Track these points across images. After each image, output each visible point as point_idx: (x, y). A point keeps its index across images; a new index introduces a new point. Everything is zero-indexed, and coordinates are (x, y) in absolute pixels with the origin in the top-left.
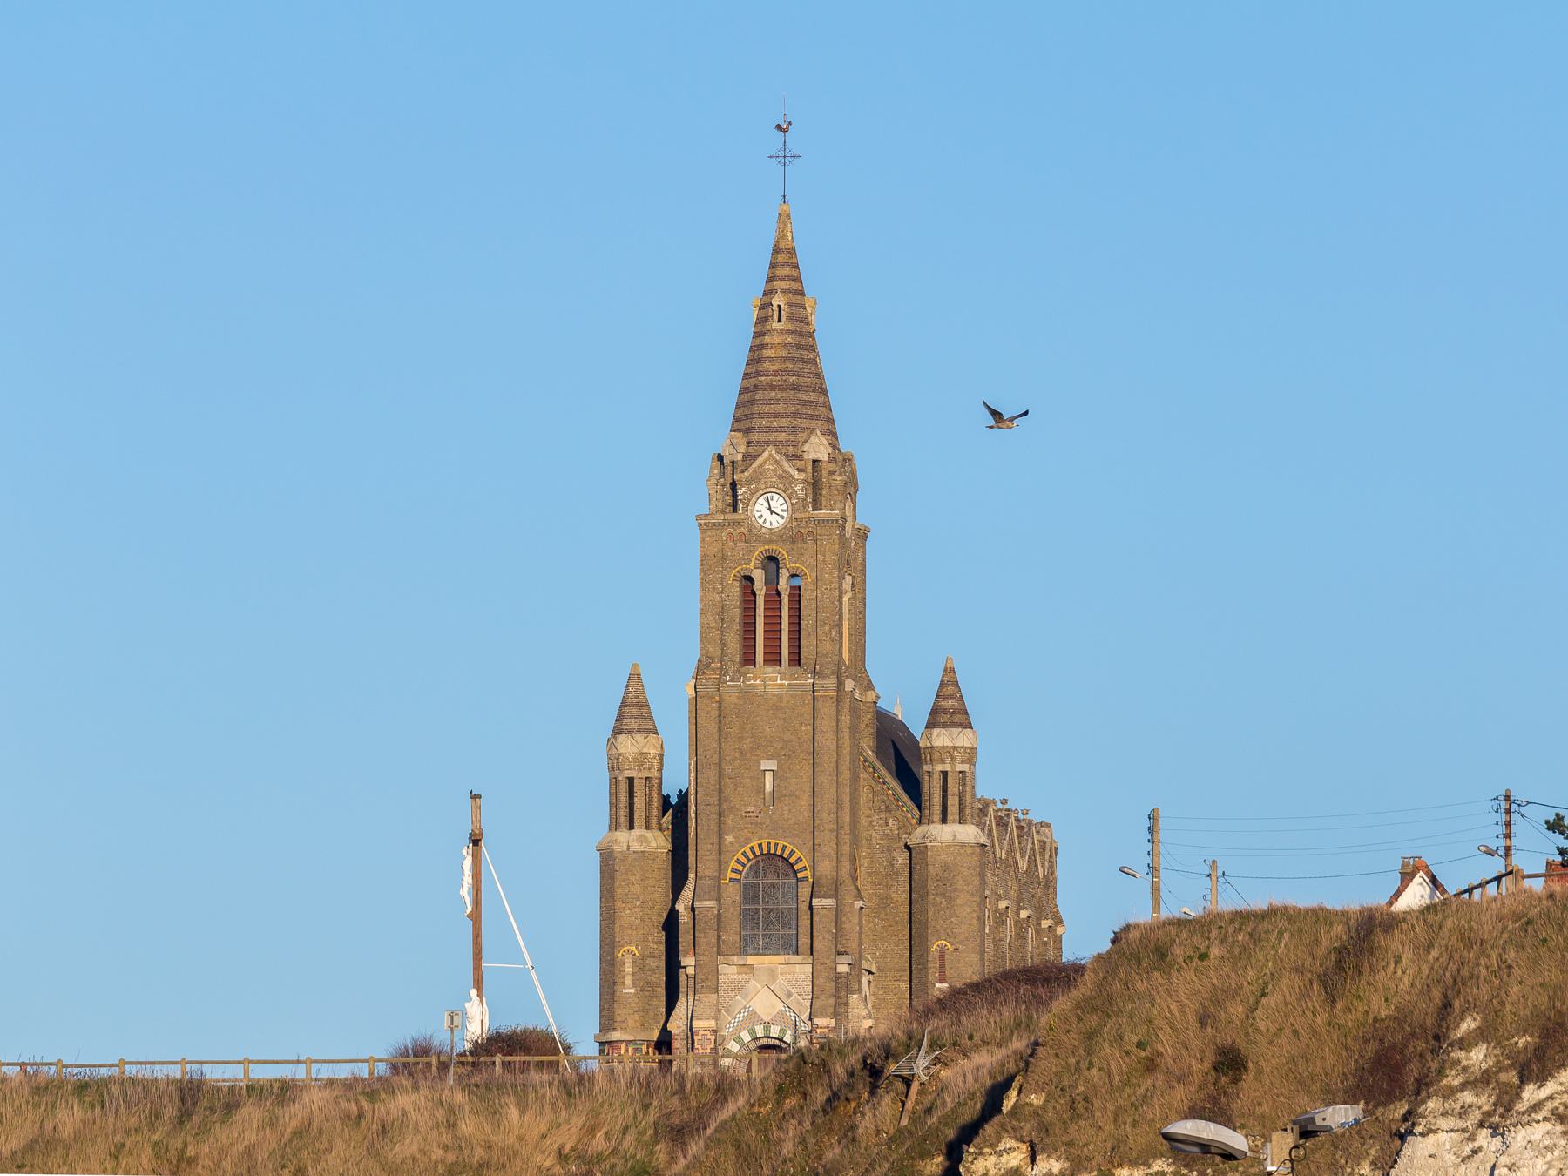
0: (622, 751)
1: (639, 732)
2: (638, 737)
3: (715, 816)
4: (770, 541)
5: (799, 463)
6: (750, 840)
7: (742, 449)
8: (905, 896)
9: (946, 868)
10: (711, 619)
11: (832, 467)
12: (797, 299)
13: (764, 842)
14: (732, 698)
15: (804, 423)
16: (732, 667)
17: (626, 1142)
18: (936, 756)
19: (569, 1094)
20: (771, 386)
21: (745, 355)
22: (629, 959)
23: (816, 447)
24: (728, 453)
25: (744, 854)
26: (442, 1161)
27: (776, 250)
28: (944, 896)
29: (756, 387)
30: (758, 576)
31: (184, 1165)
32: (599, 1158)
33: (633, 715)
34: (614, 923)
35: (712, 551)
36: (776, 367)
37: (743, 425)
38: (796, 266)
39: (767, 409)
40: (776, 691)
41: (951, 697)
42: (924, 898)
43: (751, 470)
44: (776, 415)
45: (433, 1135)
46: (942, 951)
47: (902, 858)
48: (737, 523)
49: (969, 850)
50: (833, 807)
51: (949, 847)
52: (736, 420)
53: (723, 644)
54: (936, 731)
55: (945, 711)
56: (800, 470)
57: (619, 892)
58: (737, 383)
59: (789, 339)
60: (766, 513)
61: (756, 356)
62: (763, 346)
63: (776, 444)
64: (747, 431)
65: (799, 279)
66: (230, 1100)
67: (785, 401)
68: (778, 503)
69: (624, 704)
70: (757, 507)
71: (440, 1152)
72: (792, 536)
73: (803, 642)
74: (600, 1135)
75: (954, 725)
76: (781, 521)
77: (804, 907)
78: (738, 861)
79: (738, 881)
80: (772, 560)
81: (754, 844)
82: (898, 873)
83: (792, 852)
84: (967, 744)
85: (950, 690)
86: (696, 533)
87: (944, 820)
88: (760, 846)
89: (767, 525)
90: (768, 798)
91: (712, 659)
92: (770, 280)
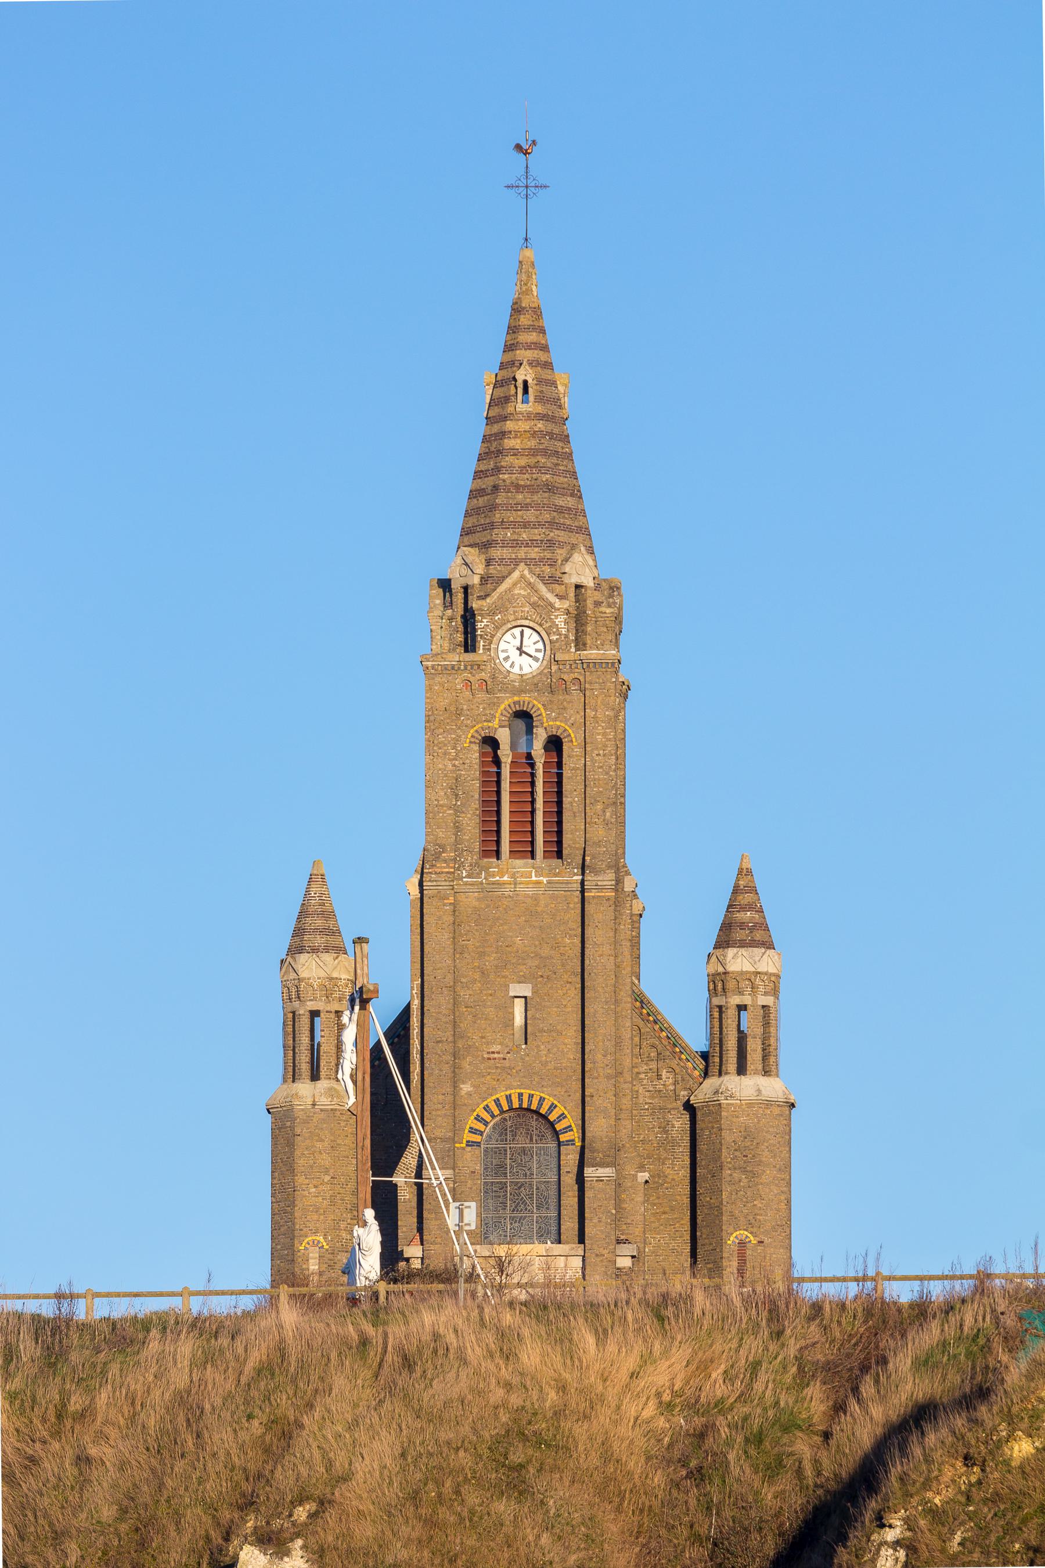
0: (303, 974)
1: (327, 950)
2: (328, 957)
3: (449, 1058)
4: (521, 691)
5: (558, 589)
6: (495, 1090)
7: (480, 569)
8: (685, 1173)
9: (747, 1134)
10: (442, 795)
11: (598, 596)
12: (546, 374)
13: (514, 1093)
14: (470, 900)
15: (561, 536)
16: (470, 859)
17: (758, 1386)
18: (731, 985)
19: (661, 1319)
21: (476, 447)
22: (314, 1254)
23: (580, 570)
24: (458, 576)
25: (487, 1108)
26: (504, 1404)
27: (517, 309)
28: (744, 1171)
29: (496, 488)
30: (503, 736)
31: (68, 1423)
32: (720, 1406)
33: (312, 928)
34: (293, 1204)
35: (442, 703)
36: (523, 461)
37: (477, 538)
38: (542, 331)
39: (512, 516)
40: (530, 891)
41: (750, 907)
42: (716, 1174)
43: (495, 595)
44: (526, 525)
45: (488, 1365)
46: (742, 1244)
47: (680, 1123)
48: (478, 666)
49: (777, 1111)
50: (610, 1045)
51: (750, 1105)
52: (466, 532)
53: (458, 828)
54: (731, 952)
55: (742, 925)
56: (561, 597)
57: (301, 1163)
58: (467, 483)
59: (540, 425)
61: (492, 448)
62: (503, 434)
63: (528, 562)
64: (485, 546)
65: (545, 348)
66: (123, 1337)
67: (538, 507)
68: (532, 641)
69: (303, 913)
70: (502, 646)
71: (501, 1392)
72: (552, 683)
73: (566, 826)
74: (717, 1374)
75: (753, 944)
76: (536, 665)
77: (569, 1180)
78: (478, 1118)
79: (478, 1144)
80: (524, 716)
81: (501, 1095)
82: (674, 1143)
83: (552, 1107)
84: (772, 970)
85: (746, 898)
86: (421, 680)
87: (741, 1070)
88: (509, 1098)
89: (516, 670)
90: (519, 1035)
91: (443, 848)
92: (509, 348)
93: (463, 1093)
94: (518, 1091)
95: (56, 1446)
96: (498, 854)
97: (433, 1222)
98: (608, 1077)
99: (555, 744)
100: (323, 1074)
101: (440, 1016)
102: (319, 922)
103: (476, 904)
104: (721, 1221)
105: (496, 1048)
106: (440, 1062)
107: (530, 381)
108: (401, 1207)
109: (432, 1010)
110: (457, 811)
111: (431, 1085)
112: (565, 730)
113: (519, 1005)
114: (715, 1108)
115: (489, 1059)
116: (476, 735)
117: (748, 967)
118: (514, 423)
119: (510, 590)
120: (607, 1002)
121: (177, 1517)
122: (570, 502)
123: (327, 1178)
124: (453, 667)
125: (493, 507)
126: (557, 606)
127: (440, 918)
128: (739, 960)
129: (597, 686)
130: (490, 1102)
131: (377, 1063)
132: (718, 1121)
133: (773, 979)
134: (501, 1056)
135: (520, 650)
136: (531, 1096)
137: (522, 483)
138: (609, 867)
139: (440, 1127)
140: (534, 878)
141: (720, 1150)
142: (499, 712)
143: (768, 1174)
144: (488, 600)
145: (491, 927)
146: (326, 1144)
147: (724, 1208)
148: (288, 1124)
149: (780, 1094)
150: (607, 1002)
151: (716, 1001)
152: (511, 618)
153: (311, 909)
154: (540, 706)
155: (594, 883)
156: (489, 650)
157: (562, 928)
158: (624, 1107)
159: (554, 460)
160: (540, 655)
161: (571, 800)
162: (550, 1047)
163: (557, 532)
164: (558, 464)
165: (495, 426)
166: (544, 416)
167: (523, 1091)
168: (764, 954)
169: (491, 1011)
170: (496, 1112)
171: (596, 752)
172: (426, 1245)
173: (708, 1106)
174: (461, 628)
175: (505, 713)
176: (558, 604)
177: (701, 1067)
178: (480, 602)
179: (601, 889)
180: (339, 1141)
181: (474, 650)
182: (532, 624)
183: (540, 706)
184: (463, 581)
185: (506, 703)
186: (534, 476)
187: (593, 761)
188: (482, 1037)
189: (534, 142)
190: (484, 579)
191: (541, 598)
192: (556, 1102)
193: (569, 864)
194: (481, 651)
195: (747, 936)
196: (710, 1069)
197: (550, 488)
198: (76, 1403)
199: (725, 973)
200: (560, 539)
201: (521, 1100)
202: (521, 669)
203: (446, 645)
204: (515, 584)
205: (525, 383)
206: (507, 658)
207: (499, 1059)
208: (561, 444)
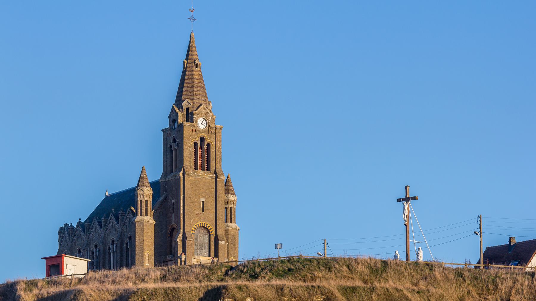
4: (202, 133)
9: (234, 236)
18: (229, 202)
36: (198, 81)
39: (197, 93)
44: (200, 95)
57: (145, 234)
81: (199, 223)
99: (208, 145)
135: (202, 123)
179: (220, 178)
181: (193, 122)
184: (187, 107)
190: (193, 107)
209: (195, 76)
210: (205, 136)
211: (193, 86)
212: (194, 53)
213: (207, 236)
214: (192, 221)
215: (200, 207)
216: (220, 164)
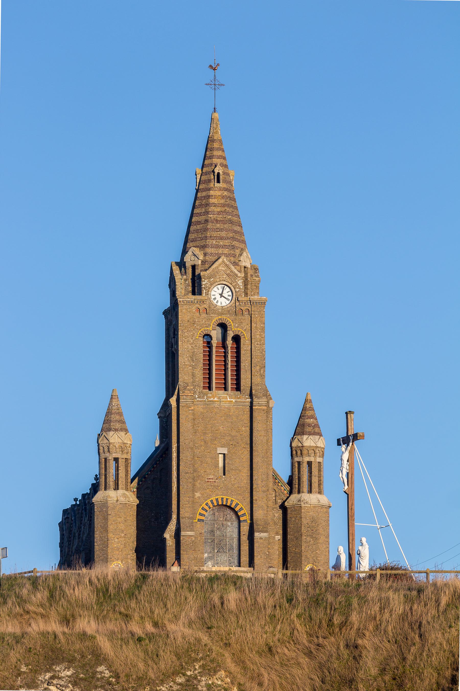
1: (121, 430)
2: (123, 433)
4: (222, 314)
7: (201, 257)
9: (313, 520)
13: (219, 497)
18: (305, 452)
20: (217, 221)
25: (207, 504)
28: (312, 537)
33: (111, 421)
34: (107, 546)
39: (215, 234)
42: (299, 537)
44: (221, 238)
47: (278, 514)
51: (314, 507)
53: (193, 375)
56: (240, 272)
59: (226, 193)
60: (218, 297)
63: (227, 255)
67: (227, 230)
70: (213, 293)
72: (236, 311)
75: (315, 434)
76: (228, 302)
78: (203, 509)
80: (223, 326)
81: (214, 498)
83: (237, 505)
87: (310, 491)
88: (217, 500)
93: (196, 497)
94: (221, 497)
95: (333, 639)
96: (210, 388)
97: (185, 556)
98: (264, 492)
99: (237, 339)
100: (120, 487)
101: (187, 461)
102: (118, 417)
103: (202, 410)
104: (301, 560)
105: (211, 477)
106: (187, 482)
107: (221, 173)
108: (168, 548)
109: (184, 458)
110: (194, 367)
111: (183, 493)
112: (242, 332)
113: (221, 456)
114: (298, 508)
115: (208, 482)
116: (202, 333)
117: (313, 444)
118: (213, 191)
119: (217, 267)
120: (263, 457)
121: (420, 675)
122: (237, 228)
123: (123, 535)
124: (192, 302)
125: (206, 230)
126: (239, 275)
127: (187, 416)
128: (309, 441)
129: (257, 313)
130: (209, 501)
131: (140, 483)
132: (300, 514)
133: (322, 450)
134: (214, 480)
135: (221, 295)
136: (227, 499)
137: (219, 219)
138: (264, 396)
139: (187, 512)
140: (229, 400)
141: (301, 527)
142: (212, 323)
143: (322, 539)
144: (208, 272)
145: (209, 421)
146: (122, 519)
147: (303, 554)
148: (105, 509)
149: (327, 503)
150: (263, 457)
151: (296, 459)
152: (218, 280)
153: (113, 411)
154: (231, 321)
155: (258, 402)
156: (208, 294)
157: (241, 423)
158: (269, 506)
159: (232, 209)
160: (230, 298)
161: (245, 364)
162: (236, 477)
163: (235, 242)
164: (233, 211)
165: (204, 193)
166: (227, 189)
167: (223, 497)
168: (319, 438)
169: (209, 460)
170: (211, 506)
171: (256, 343)
172: (182, 566)
173: (295, 507)
174: (191, 284)
175: (214, 323)
176: (239, 275)
177: (288, 489)
178: (204, 272)
179: (260, 405)
180: (128, 518)
181: (200, 294)
182: (227, 283)
183: (231, 321)
184: (193, 263)
185: (216, 319)
186: (224, 216)
187: (255, 347)
188: (205, 472)
189: (218, 64)
190: (203, 262)
191: (232, 271)
192: (238, 502)
193: (244, 394)
194: (204, 295)
195: (312, 430)
196: (294, 490)
197: (231, 222)
198: (337, 620)
199: (302, 447)
200: (237, 245)
201: (222, 501)
202: (221, 303)
203: (183, 292)
204: (220, 265)
205: (218, 174)
206: (215, 299)
207: (213, 482)
208: (233, 202)
209: (212, 201)
210: (228, 320)
211: (206, 221)
212: (216, 153)
213: (236, 524)
214: (197, 495)
215: (217, 466)
216: (263, 376)
